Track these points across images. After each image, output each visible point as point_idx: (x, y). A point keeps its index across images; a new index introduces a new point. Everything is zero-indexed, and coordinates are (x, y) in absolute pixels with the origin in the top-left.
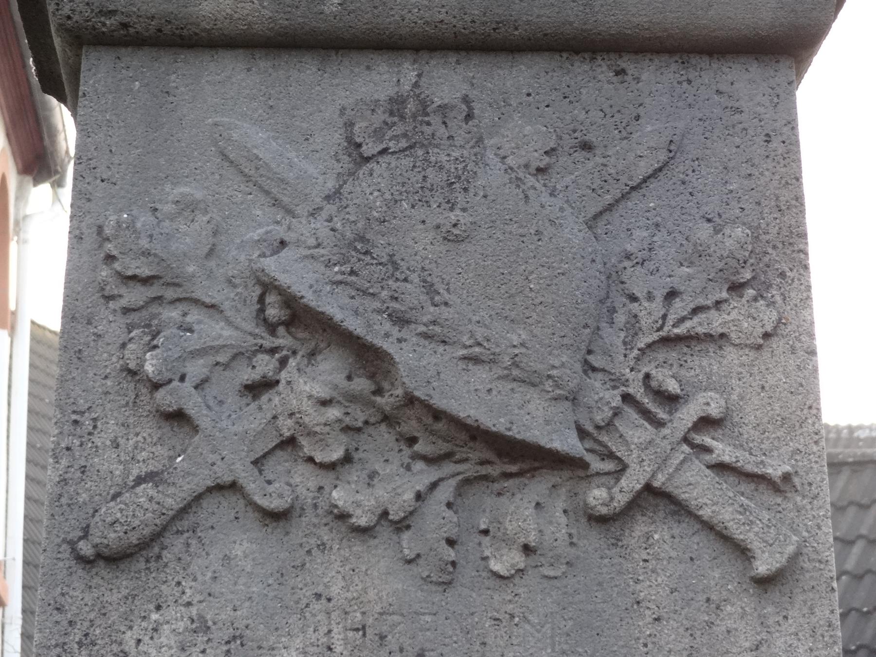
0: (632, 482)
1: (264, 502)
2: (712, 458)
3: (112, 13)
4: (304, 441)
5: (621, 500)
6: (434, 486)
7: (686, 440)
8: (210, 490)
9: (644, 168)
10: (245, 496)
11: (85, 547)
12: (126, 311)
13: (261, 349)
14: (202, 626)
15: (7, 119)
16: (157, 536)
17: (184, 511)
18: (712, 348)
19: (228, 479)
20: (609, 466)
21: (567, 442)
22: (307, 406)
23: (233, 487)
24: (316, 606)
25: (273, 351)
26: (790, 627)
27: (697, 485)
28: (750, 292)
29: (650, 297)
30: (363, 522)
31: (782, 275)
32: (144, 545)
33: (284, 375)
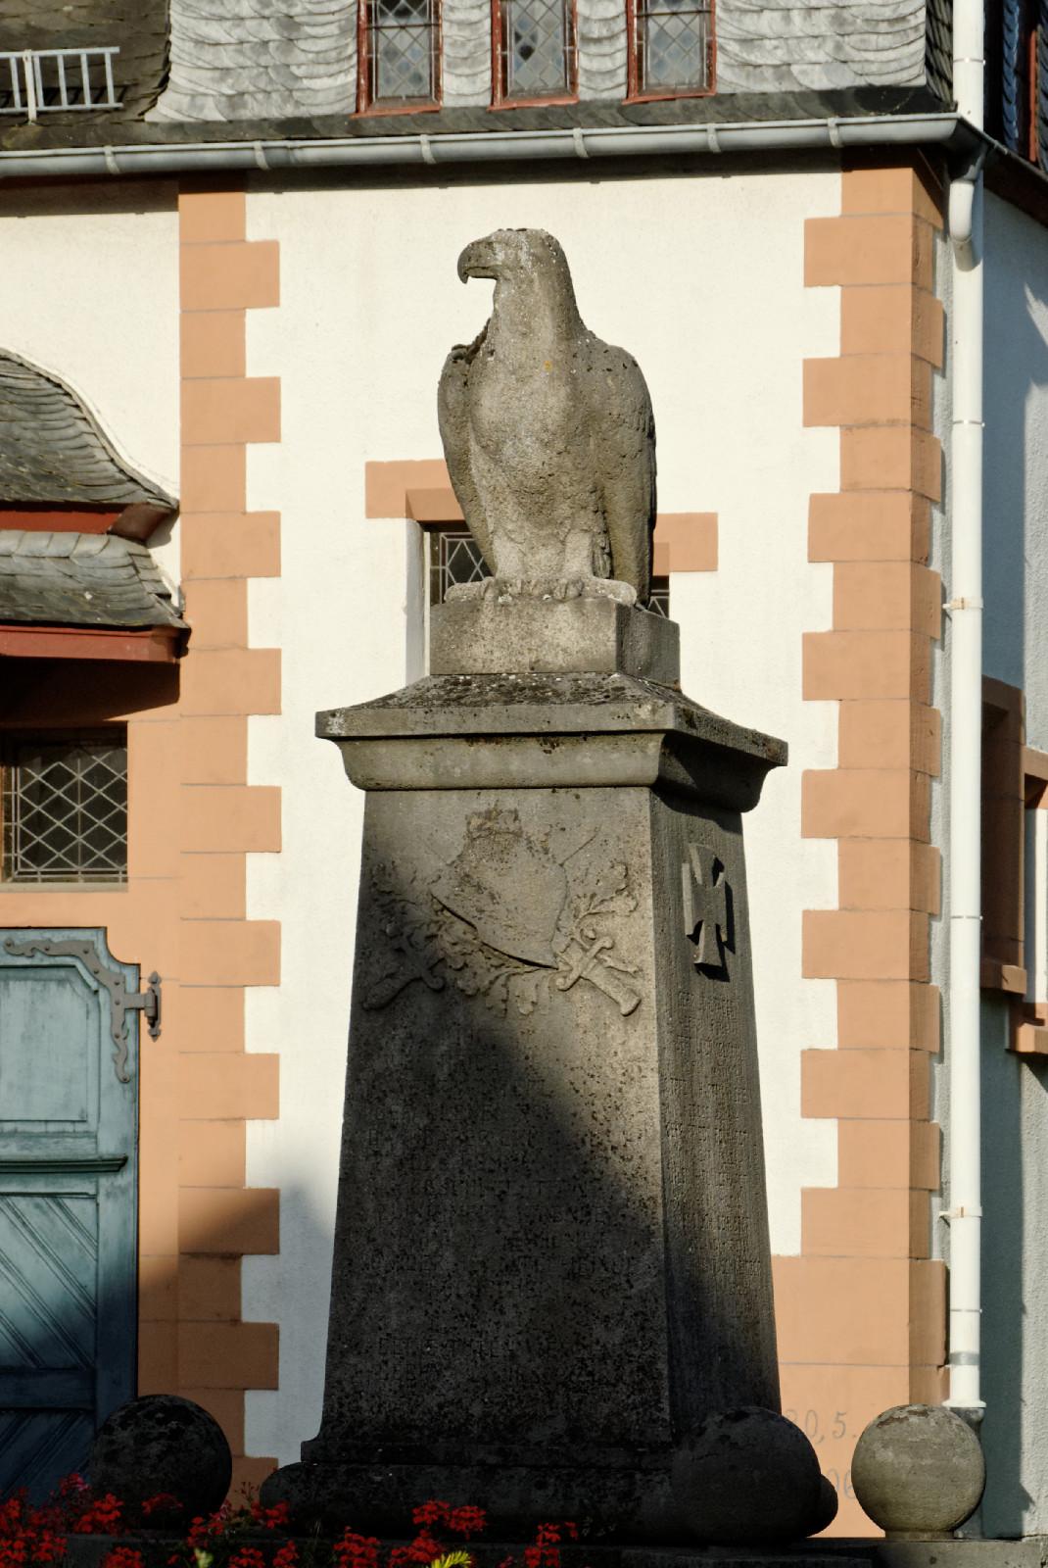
0: (574, 976)
1: (431, 985)
2: (606, 965)
3: (545, 751)
4: (448, 960)
5: (569, 982)
6: (497, 978)
7: (595, 957)
8: (412, 980)
9: (584, 840)
10: (594, 987)
11: (365, 1005)
12: (382, 906)
13: (432, 921)
14: (411, 1036)
15: (944, 748)
16: (393, 999)
17: (402, 989)
18: (610, 916)
19: (418, 976)
20: (567, 968)
21: (548, 960)
22: (447, 945)
23: (420, 979)
24: (454, 1028)
25: (437, 922)
26: (636, 1034)
27: (598, 977)
28: (626, 893)
29: (585, 896)
30: (470, 993)
31: (640, 885)
32: (388, 1004)
33: (440, 933)
